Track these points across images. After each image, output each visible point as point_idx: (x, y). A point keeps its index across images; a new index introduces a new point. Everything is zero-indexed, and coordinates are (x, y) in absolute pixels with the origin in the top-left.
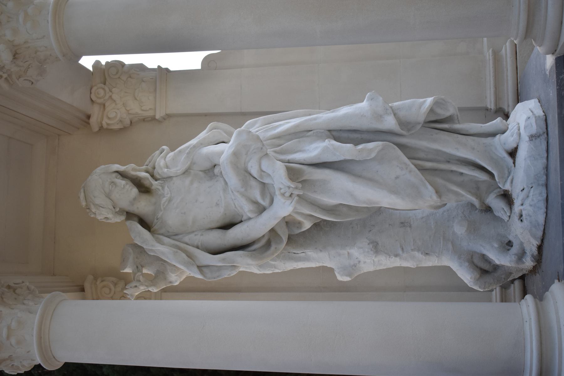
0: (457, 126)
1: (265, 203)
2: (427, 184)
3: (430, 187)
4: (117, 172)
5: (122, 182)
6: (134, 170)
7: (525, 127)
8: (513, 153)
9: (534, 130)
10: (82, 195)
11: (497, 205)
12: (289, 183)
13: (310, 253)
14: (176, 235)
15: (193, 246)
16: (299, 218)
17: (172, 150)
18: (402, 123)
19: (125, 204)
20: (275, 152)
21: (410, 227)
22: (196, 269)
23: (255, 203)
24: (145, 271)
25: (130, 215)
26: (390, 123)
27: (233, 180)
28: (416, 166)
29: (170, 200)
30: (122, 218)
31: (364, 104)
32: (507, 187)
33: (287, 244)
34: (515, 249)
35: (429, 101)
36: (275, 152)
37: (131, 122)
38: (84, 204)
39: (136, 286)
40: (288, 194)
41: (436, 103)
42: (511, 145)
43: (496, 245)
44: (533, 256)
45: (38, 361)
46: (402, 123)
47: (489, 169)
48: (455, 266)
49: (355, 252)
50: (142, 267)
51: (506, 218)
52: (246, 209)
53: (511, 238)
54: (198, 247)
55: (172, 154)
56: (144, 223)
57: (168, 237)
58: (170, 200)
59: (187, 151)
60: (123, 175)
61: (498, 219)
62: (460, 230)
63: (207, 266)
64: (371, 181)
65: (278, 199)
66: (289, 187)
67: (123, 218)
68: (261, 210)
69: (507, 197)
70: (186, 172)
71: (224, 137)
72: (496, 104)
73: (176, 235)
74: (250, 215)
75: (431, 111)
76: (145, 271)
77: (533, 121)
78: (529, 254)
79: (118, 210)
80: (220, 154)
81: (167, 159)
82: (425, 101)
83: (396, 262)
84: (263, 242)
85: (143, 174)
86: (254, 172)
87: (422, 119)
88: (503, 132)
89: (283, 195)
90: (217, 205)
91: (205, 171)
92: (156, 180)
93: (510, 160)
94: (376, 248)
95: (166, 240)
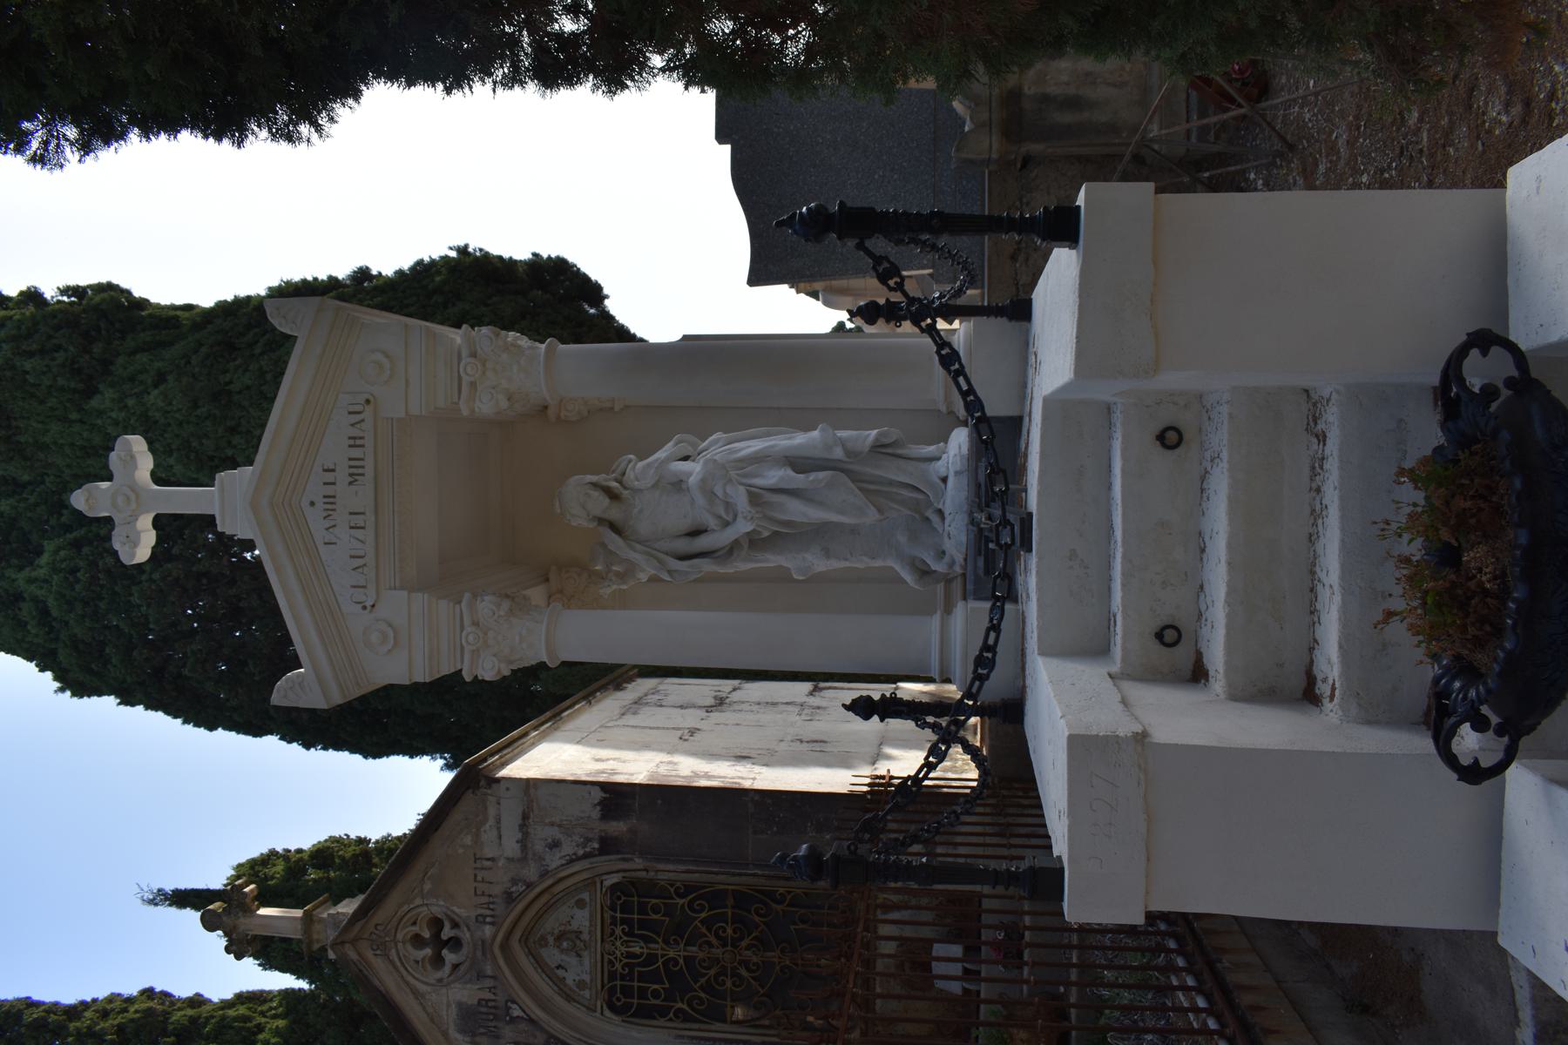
0: (900, 451)
1: (729, 518)
2: (870, 505)
3: (872, 508)
4: (591, 483)
5: (596, 494)
6: (606, 480)
7: (952, 463)
8: (944, 480)
9: (958, 467)
10: (557, 504)
11: (935, 519)
12: (749, 508)
13: (769, 556)
14: (647, 541)
15: (663, 552)
16: (759, 529)
17: (641, 460)
18: (848, 453)
19: (598, 512)
20: (738, 475)
21: (859, 534)
22: (666, 574)
23: (720, 517)
24: (614, 568)
25: (601, 521)
26: (838, 453)
27: (701, 501)
28: (860, 489)
29: (641, 511)
30: (593, 525)
31: (815, 434)
32: (940, 506)
33: (749, 547)
34: (947, 559)
35: (874, 432)
36: (738, 475)
37: (589, 412)
38: (559, 511)
39: (609, 586)
40: (749, 518)
41: (879, 434)
42: (943, 472)
43: (932, 554)
44: (961, 565)
45: (545, 659)
46: (848, 453)
47: (925, 491)
48: (898, 568)
49: (809, 556)
50: (612, 564)
51: (941, 532)
52: (712, 523)
53: (944, 548)
54: (667, 554)
55: (641, 464)
56: (615, 528)
57: (639, 543)
58: (641, 511)
59: (656, 465)
60: (595, 485)
61: (935, 529)
62: (902, 538)
63: (676, 571)
64: (821, 504)
65: (740, 518)
66: (750, 512)
67: (595, 524)
68: (726, 524)
69: (940, 513)
70: (655, 486)
71: (689, 451)
72: (948, 408)
73: (647, 541)
74: (715, 528)
75: (877, 439)
76: (614, 568)
77: (958, 458)
78: (957, 563)
79: (591, 517)
80: (689, 474)
81: (636, 471)
82: (869, 435)
83: (847, 564)
84: (725, 551)
85: (614, 484)
86: (720, 493)
87: (867, 450)
88: (939, 459)
89: (745, 518)
90: (685, 517)
91: (673, 484)
92: (625, 488)
93: (943, 486)
94: (827, 554)
95: (638, 547)
